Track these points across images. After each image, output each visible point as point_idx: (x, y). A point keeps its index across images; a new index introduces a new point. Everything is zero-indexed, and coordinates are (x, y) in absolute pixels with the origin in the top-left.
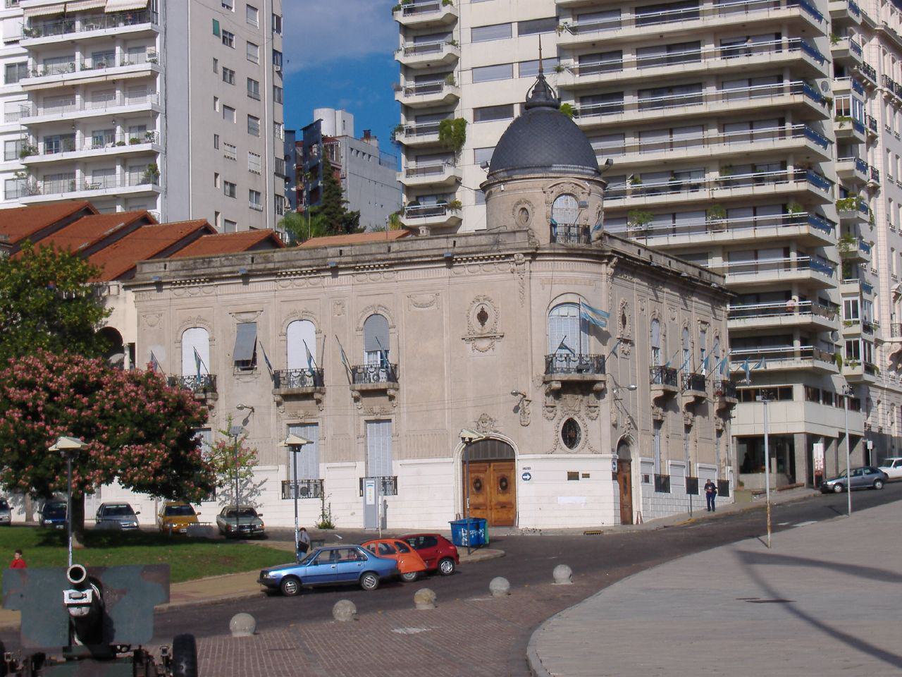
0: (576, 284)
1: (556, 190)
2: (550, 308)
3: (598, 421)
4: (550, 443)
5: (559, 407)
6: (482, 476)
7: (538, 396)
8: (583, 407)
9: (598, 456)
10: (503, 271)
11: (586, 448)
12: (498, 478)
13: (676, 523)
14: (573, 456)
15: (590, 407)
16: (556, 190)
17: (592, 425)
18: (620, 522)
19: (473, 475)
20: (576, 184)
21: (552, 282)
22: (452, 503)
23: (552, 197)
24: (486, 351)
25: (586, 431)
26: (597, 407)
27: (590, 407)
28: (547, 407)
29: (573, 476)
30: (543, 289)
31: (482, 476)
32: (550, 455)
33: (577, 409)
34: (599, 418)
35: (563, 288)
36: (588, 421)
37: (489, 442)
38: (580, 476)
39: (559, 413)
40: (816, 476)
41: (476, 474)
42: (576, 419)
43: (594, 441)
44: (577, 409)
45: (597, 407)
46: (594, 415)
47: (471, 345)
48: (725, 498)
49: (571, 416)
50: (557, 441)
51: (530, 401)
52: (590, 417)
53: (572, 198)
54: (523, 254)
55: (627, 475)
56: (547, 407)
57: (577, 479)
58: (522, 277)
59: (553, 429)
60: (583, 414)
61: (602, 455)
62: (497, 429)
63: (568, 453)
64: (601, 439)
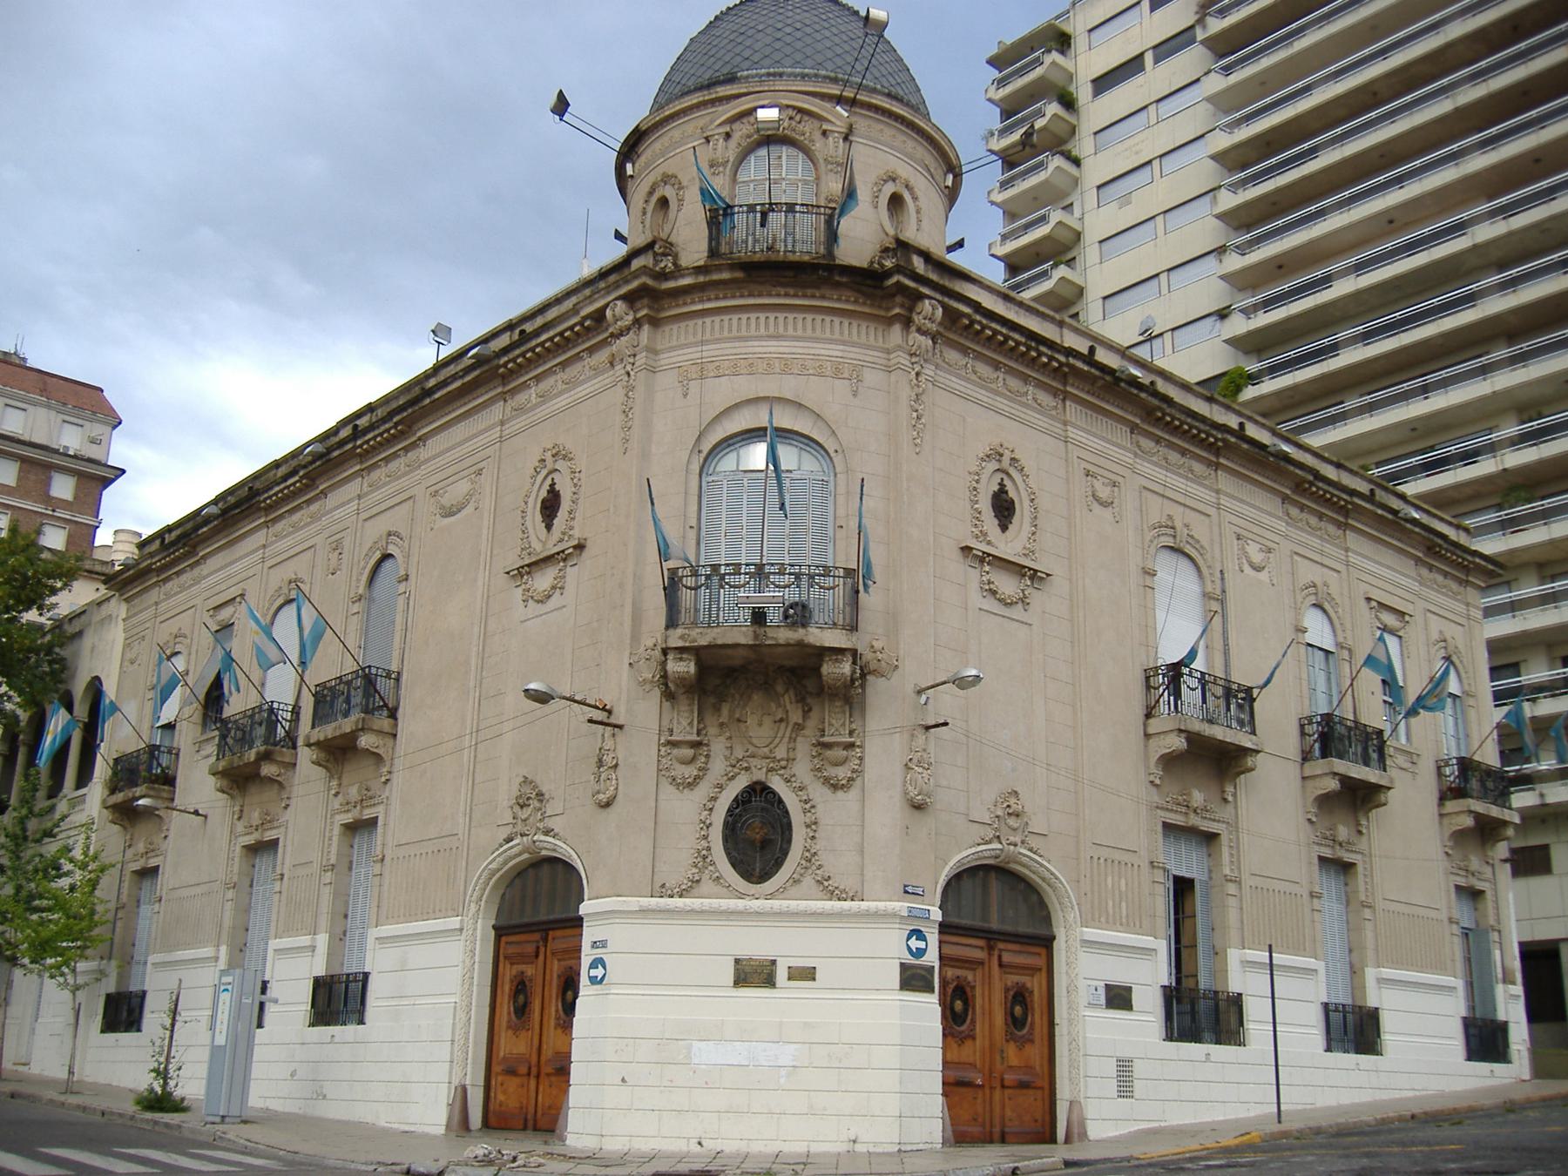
0: (785, 372)
1: (741, 130)
2: (706, 446)
3: (854, 793)
4: (677, 863)
5: (718, 747)
6: (529, 970)
7: (644, 714)
8: (803, 748)
9: (855, 905)
10: (597, 371)
11: (808, 881)
12: (1007, 990)
13: (1487, 1102)
14: (755, 904)
15: (828, 746)
16: (741, 130)
17: (834, 810)
18: (938, 1137)
19: (1013, 979)
20: (800, 110)
21: (702, 370)
22: (444, 1052)
23: (732, 151)
24: (549, 596)
25: (812, 825)
26: (852, 746)
27: (828, 746)
28: (674, 744)
29: (754, 974)
30: (685, 396)
31: (529, 970)
32: (677, 902)
33: (781, 753)
34: (858, 782)
35: (747, 387)
36: (818, 792)
37: (546, 868)
38: (781, 974)
39: (718, 766)
40: (932, 991)
41: (959, 972)
42: (777, 784)
43: (839, 864)
44: (781, 753)
45: (852, 746)
46: (842, 773)
47: (520, 590)
48: (1495, 1066)
49: (759, 775)
50: (704, 857)
51: (620, 727)
52: (826, 781)
53: (792, 151)
54: (622, 298)
55: (1035, 984)
56: (674, 744)
57: (769, 981)
58: (629, 368)
59: (693, 816)
60: (802, 769)
61: (864, 905)
62: (550, 823)
63: (742, 896)
64: (862, 852)
